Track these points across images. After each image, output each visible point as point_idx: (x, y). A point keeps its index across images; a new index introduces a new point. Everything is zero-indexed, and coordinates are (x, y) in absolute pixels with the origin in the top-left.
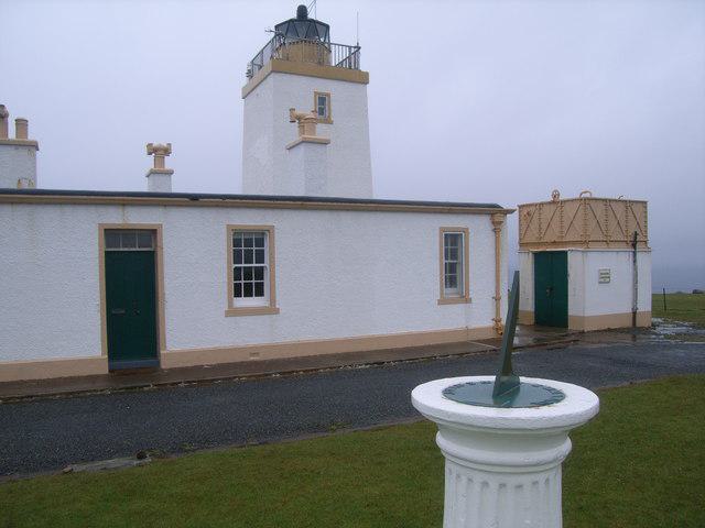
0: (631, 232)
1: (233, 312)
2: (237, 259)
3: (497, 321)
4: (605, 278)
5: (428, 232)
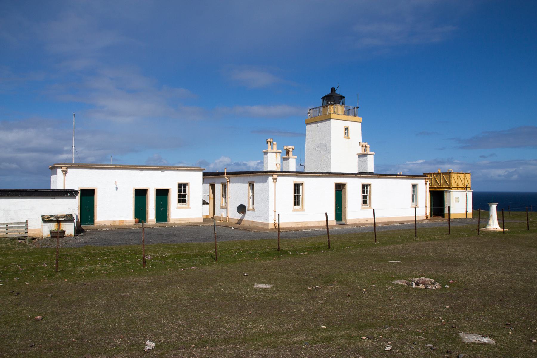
0: (465, 185)
1: (295, 210)
2: (295, 193)
3: (426, 214)
4: (457, 200)
5: (408, 183)
